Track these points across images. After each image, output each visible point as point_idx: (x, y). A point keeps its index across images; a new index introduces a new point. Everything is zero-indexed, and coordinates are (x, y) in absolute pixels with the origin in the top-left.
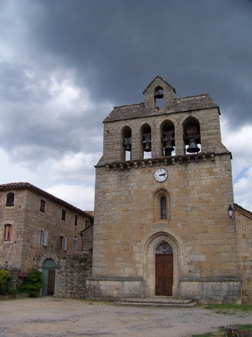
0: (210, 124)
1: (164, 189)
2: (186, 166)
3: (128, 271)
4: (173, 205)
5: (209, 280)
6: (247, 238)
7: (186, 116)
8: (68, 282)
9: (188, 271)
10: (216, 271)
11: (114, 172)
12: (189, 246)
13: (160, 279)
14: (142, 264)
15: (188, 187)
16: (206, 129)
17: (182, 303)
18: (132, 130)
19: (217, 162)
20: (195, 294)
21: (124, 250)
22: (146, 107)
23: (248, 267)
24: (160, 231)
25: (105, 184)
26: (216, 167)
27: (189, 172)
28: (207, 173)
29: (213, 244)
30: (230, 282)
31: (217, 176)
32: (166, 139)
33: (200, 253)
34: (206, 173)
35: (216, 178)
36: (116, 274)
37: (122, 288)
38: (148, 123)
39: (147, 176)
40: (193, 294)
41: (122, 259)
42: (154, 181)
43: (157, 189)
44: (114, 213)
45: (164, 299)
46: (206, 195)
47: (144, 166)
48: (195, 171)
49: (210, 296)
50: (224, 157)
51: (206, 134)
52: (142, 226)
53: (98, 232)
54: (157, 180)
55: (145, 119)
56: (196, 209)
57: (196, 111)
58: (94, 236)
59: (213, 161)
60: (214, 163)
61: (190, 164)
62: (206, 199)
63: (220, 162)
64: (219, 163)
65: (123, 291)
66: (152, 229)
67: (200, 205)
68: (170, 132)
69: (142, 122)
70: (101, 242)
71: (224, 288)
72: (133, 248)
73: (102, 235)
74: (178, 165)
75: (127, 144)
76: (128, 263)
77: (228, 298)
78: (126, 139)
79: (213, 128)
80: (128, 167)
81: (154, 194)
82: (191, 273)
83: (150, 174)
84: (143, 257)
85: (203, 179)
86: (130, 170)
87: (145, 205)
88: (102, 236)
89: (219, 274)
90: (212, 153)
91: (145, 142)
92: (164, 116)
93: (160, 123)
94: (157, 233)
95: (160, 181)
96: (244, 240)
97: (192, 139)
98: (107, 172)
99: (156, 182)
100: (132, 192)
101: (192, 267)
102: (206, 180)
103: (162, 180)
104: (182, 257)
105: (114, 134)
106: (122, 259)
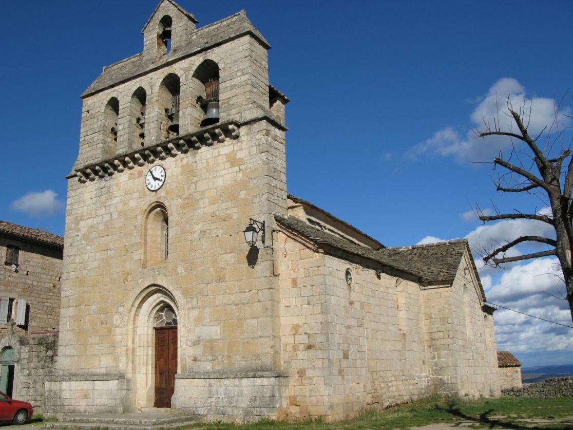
3: (104, 364)
5: (221, 375)
7: (198, 60)
9: (193, 358)
10: (238, 358)
13: (161, 374)
14: (125, 348)
15: (196, 194)
19: (243, 138)
20: (199, 405)
23: (301, 347)
26: (241, 149)
27: (199, 165)
28: (227, 162)
30: (255, 379)
31: (242, 167)
35: (240, 170)
39: (136, 183)
40: (192, 402)
41: (97, 340)
44: (88, 257)
46: (224, 206)
48: (207, 163)
49: (222, 408)
51: (229, 88)
54: (149, 187)
56: (207, 235)
58: (62, 300)
60: (239, 142)
63: (249, 138)
67: (214, 226)
69: (133, 86)
72: (113, 317)
76: (105, 347)
79: (239, 74)
81: (146, 214)
82: (198, 363)
84: (127, 334)
85: (220, 176)
88: (72, 299)
89: (243, 363)
95: (153, 189)
100: (115, 216)
101: (199, 350)
102: (224, 176)
103: (157, 187)
106: (97, 340)
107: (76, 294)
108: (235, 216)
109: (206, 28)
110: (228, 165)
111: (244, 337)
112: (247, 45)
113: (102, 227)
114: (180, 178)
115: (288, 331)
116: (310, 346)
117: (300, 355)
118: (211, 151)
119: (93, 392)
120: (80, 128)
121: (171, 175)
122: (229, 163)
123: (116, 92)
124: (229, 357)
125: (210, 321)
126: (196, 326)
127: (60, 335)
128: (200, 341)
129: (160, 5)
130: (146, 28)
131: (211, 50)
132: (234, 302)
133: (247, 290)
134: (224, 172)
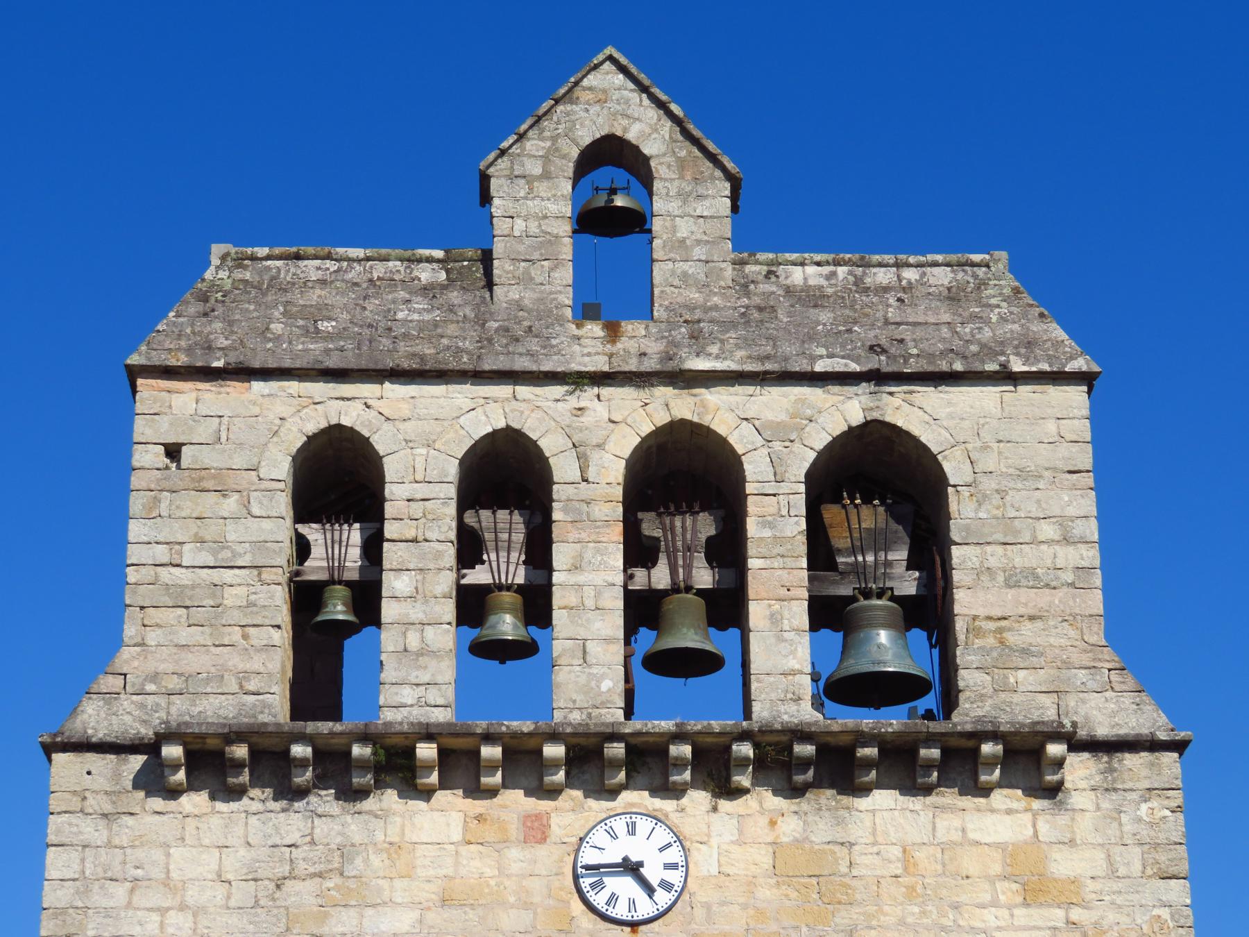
0: (1023, 501)
16: (1000, 537)
18: (392, 468)
25: (139, 900)
31: (1076, 914)
32: (660, 577)
34: (991, 880)
42: (577, 906)
63: (1106, 805)
64: (1098, 808)
68: (689, 520)
75: (324, 576)
78: (312, 532)
79: (1048, 530)
83: (542, 851)
90: (1057, 736)
91: (478, 576)
92: (664, 392)
93: (626, 443)
105: (231, 481)
109: (818, 264)
110: (1008, 891)
112: (1076, 422)
114: (767, 893)
120: (122, 517)
121: (714, 871)
122: (1015, 886)
123: (358, 405)
129: (581, 79)
130: (503, 153)
131: (905, 388)
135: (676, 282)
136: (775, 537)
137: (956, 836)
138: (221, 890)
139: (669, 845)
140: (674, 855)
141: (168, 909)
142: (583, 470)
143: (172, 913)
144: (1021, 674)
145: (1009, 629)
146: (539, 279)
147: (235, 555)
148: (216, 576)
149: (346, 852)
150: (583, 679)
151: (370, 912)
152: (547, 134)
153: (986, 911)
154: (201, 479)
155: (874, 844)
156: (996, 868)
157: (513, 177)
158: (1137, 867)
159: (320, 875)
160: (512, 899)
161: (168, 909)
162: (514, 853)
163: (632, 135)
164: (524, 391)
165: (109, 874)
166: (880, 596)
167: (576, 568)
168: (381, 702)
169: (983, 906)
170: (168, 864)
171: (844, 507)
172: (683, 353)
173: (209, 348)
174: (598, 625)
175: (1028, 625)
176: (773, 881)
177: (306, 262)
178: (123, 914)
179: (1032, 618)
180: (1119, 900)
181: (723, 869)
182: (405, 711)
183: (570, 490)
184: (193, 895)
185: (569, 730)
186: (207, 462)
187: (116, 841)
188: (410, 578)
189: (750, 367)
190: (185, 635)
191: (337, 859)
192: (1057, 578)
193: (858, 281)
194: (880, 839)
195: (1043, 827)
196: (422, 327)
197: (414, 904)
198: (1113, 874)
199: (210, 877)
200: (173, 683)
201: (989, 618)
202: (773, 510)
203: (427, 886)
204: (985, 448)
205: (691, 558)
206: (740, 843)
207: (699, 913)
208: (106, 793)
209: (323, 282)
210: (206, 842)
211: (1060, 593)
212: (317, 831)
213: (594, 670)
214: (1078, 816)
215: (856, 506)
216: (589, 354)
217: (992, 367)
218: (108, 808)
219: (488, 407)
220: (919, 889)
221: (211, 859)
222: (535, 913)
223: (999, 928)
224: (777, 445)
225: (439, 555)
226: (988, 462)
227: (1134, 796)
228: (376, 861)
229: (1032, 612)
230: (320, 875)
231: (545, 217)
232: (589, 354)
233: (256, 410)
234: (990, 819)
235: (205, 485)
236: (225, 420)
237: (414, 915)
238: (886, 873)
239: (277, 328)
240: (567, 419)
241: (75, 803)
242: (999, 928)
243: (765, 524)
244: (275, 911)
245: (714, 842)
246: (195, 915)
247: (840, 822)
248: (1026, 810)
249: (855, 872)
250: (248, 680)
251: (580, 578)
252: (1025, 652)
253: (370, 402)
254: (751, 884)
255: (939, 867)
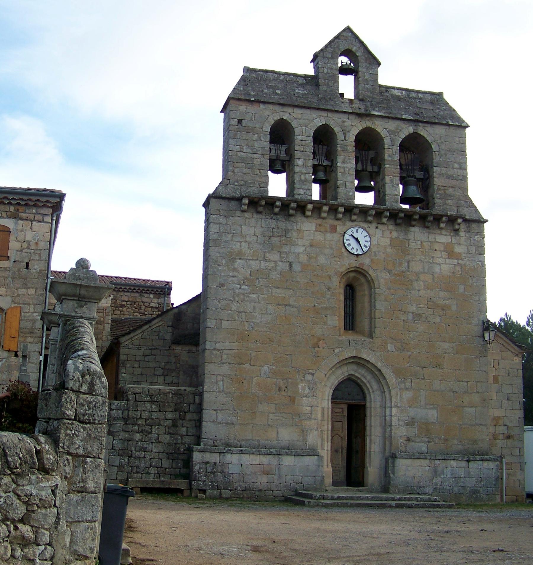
1: (362, 269)
2: (406, 233)
4: (380, 306)
5: (447, 456)
6: (500, 383)
8: (133, 456)
9: (406, 439)
10: (455, 442)
11: (255, 216)
12: (407, 389)
16: (445, 166)
17: (433, 500)
18: (297, 131)
21: (277, 389)
22: (323, 88)
23: (501, 437)
24: (354, 355)
28: (444, 251)
29: (452, 390)
31: (460, 262)
33: (428, 404)
34: (441, 251)
36: (258, 441)
37: (277, 470)
38: (332, 124)
42: (343, 250)
43: (358, 267)
45: (345, 492)
46: (442, 294)
47: (340, 216)
50: (474, 225)
52: (316, 340)
53: (218, 346)
55: (324, 114)
57: (426, 125)
59: (457, 231)
61: (412, 229)
62: (442, 302)
63: (467, 235)
64: (466, 236)
65: (280, 476)
66: (337, 350)
67: (430, 312)
70: (225, 369)
71: (472, 473)
73: (226, 352)
74: (391, 227)
75: (275, 158)
77: (479, 491)
80: (291, 212)
86: (292, 219)
87: (324, 298)
89: (460, 447)
93: (272, 121)
94: (346, 359)
96: (495, 386)
97: (413, 179)
98: (238, 213)
99: (346, 254)
100: (297, 267)
101: (412, 432)
104: (394, 411)
107: (235, 350)
108: (454, 308)
110: (445, 254)
111: (461, 423)
113: (275, 275)
114: (389, 250)
115: (86, 371)
116: (509, 436)
117: (500, 443)
118: (426, 235)
119: (279, 468)
121: (377, 244)
124: (446, 440)
125: (427, 404)
126: (410, 407)
127: (206, 396)
128: (415, 422)
132: (452, 390)
133: (465, 380)
134: (440, 260)
135: (365, 90)
136: (392, 160)
137: (434, 240)
138: (255, 238)
139: (366, 236)
140: (368, 238)
141: (242, 242)
142: (345, 137)
143: (243, 243)
144: (449, 201)
145: (447, 189)
146: (331, 85)
147: (257, 151)
148: (252, 155)
149: (286, 231)
150: (345, 192)
151: (293, 247)
152: (332, 47)
153: (439, 259)
154: (248, 130)
155: (414, 240)
156: (442, 249)
157: (324, 57)
158: (474, 251)
159: (280, 236)
160: (328, 247)
161: (242, 242)
162: (328, 235)
163: (354, 49)
164: (330, 114)
165: (227, 232)
166: (412, 177)
167: (343, 162)
168: (295, 193)
169: (439, 258)
170: (241, 230)
171: (404, 153)
172: (370, 109)
173: (250, 95)
174: (349, 178)
175: (451, 189)
176: (390, 247)
177: (269, 74)
178: (230, 242)
179: (452, 187)
180: (470, 259)
181: (379, 243)
182: (301, 196)
183: (342, 142)
184: (248, 239)
185: (346, 205)
186: (249, 125)
187: (228, 223)
188: (302, 161)
189: (387, 115)
190: (245, 170)
191: (284, 232)
192: (458, 178)
193: (408, 95)
194: (416, 239)
195: (453, 240)
196: (303, 94)
197: (303, 246)
198: (468, 252)
199: (252, 234)
200: (242, 183)
201: (442, 186)
202: (391, 153)
203: (307, 241)
204: (442, 143)
205: (367, 162)
206: (383, 237)
207: (373, 253)
208: (225, 210)
209: (274, 79)
210: (251, 225)
211: (459, 181)
212: (279, 225)
213: (348, 190)
214: (461, 238)
215: (407, 154)
216: (346, 107)
217: (445, 122)
218: (226, 215)
219: (321, 118)
220: (425, 252)
221: (252, 231)
222: (333, 250)
223: (442, 263)
224: (392, 136)
225: (309, 156)
226: (443, 147)
227: (474, 234)
228: (294, 234)
229: (452, 186)
230: (280, 236)
231: (332, 69)
232: (346, 107)
233: (262, 113)
234: (441, 236)
235: (249, 131)
236: (254, 114)
237: (304, 248)
238: (417, 247)
239: (265, 91)
240: (340, 124)
241: (217, 212)
242: (442, 263)
243: (389, 156)
244: (269, 245)
245: (377, 236)
246: (249, 244)
247: (406, 234)
248: (449, 235)
249: (410, 247)
250: (261, 184)
251: (345, 165)
252: (450, 196)
253: (291, 113)
254: (385, 247)
255: (429, 247)
